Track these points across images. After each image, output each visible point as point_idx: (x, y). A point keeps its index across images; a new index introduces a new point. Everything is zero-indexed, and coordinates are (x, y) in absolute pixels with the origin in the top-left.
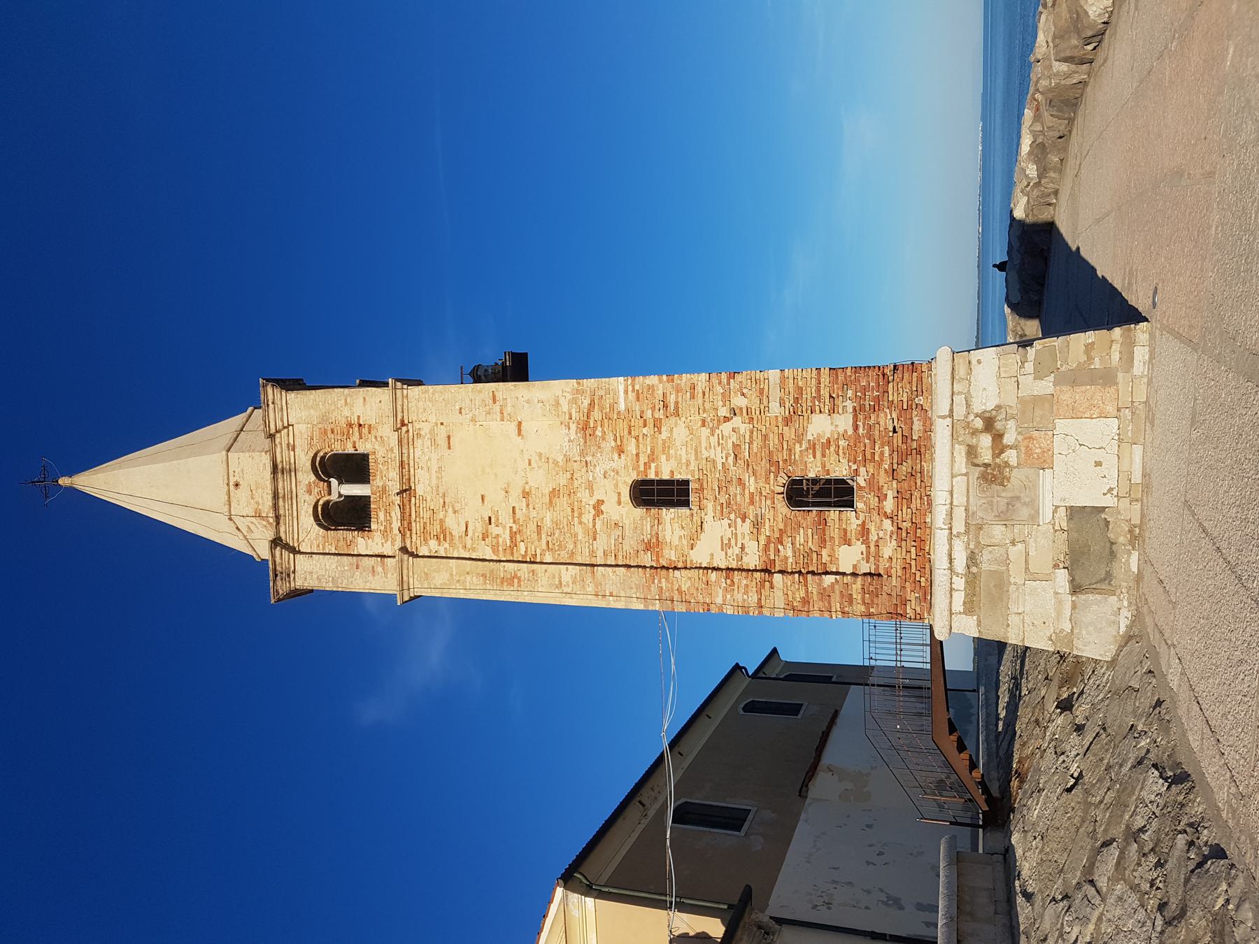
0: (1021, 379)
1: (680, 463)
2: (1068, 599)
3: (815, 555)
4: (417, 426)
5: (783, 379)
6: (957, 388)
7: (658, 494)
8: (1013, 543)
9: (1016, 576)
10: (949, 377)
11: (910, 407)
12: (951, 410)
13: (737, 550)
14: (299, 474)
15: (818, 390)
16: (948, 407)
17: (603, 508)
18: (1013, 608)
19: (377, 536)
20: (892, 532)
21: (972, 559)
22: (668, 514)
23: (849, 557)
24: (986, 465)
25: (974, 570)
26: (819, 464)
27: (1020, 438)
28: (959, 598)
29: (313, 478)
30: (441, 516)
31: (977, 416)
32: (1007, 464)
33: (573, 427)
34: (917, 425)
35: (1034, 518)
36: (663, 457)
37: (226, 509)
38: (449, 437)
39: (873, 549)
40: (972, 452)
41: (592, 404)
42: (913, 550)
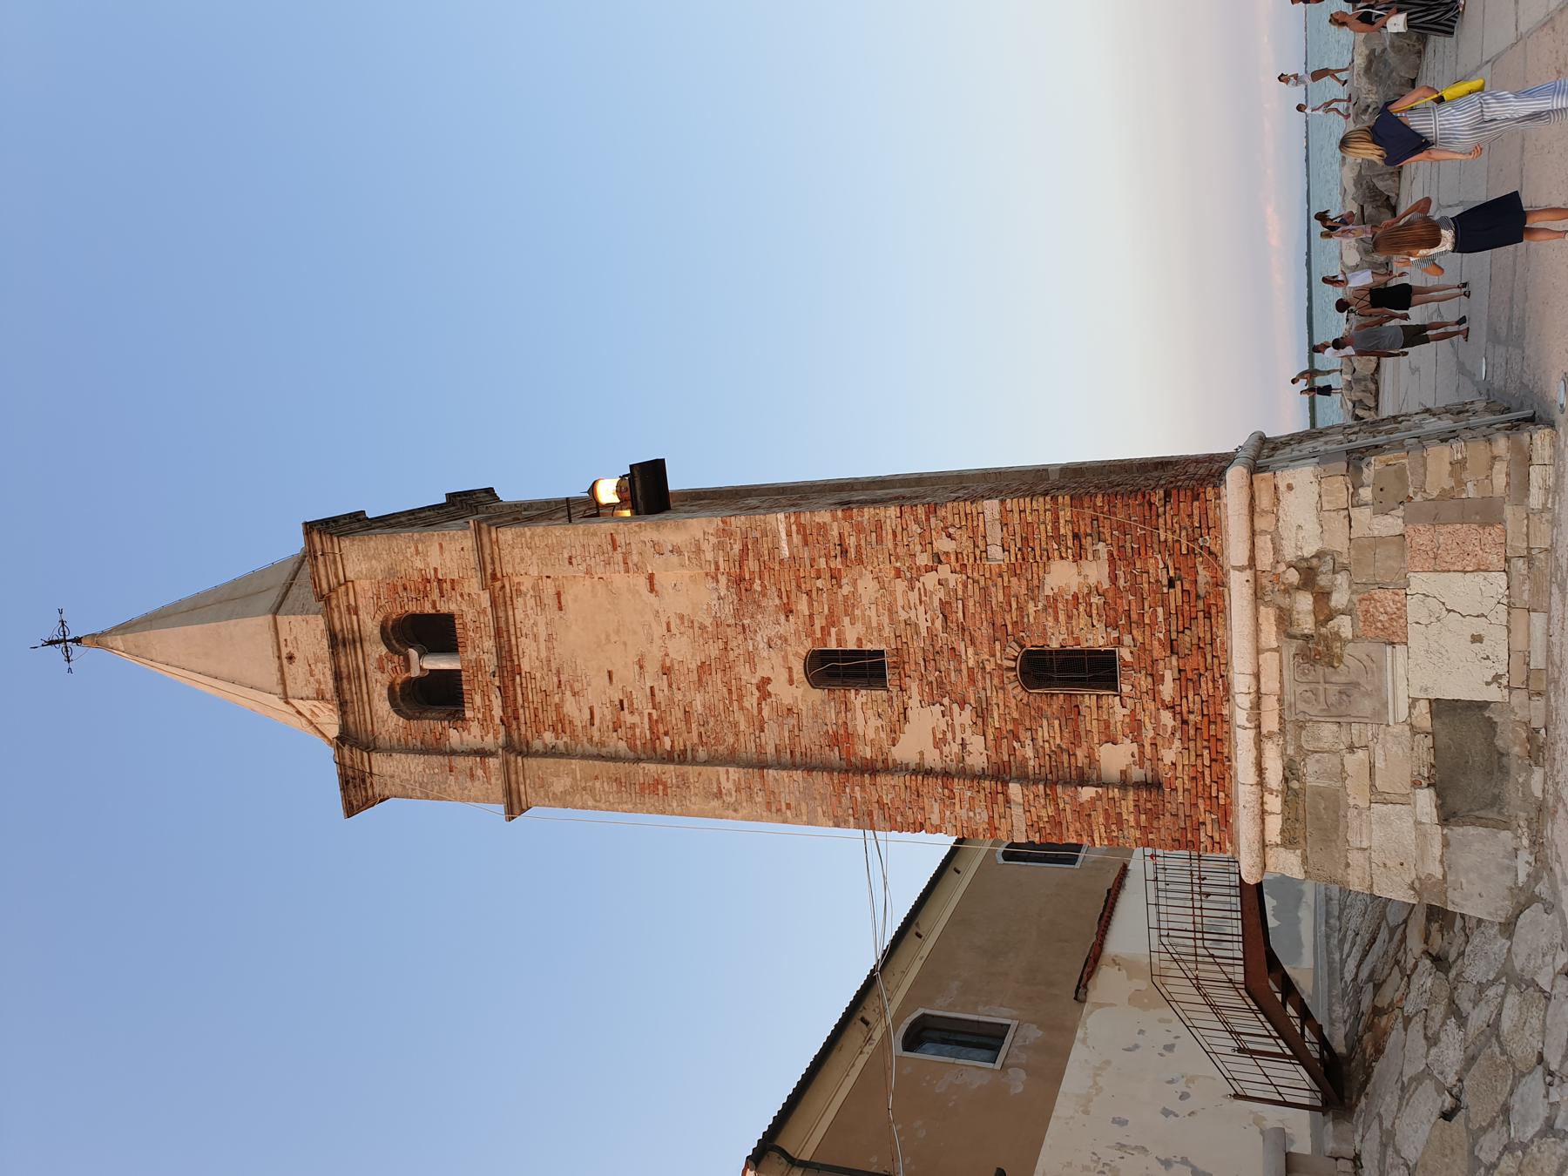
0: (1355, 512)
1: (869, 627)
2: (1437, 832)
3: (1065, 757)
4: (516, 580)
5: (1004, 512)
6: (1261, 524)
7: (840, 669)
8: (1351, 749)
9: (1356, 794)
10: (1245, 511)
11: (1191, 551)
12: (1252, 559)
13: (956, 748)
14: (367, 645)
15: (1056, 528)
16: (1247, 554)
17: (770, 688)
18: (1354, 840)
19: (475, 728)
20: (1174, 728)
21: (1291, 772)
22: (860, 698)
23: (1116, 758)
24: (1307, 638)
25: (1295, 785)
26: (1063, 630)
27: (1355, 598)
28: (1274, 825)
29: (383, 650)
30: (557, 699)
31: (1289, 566)
32: (1337, 636)
33: (723, 580)
34: (1203, 575)
35: (1379, 715)
36: (847, 620)
37: (279, 689)
38: (559, 594)
39: (1148, 748)
40: (1285, 619)
41: (744, 551)
42: (1206, 752)
